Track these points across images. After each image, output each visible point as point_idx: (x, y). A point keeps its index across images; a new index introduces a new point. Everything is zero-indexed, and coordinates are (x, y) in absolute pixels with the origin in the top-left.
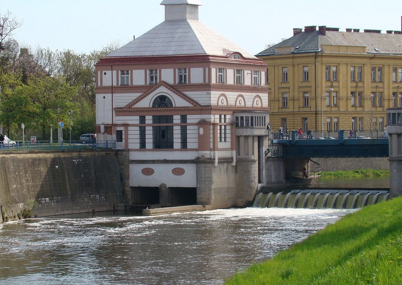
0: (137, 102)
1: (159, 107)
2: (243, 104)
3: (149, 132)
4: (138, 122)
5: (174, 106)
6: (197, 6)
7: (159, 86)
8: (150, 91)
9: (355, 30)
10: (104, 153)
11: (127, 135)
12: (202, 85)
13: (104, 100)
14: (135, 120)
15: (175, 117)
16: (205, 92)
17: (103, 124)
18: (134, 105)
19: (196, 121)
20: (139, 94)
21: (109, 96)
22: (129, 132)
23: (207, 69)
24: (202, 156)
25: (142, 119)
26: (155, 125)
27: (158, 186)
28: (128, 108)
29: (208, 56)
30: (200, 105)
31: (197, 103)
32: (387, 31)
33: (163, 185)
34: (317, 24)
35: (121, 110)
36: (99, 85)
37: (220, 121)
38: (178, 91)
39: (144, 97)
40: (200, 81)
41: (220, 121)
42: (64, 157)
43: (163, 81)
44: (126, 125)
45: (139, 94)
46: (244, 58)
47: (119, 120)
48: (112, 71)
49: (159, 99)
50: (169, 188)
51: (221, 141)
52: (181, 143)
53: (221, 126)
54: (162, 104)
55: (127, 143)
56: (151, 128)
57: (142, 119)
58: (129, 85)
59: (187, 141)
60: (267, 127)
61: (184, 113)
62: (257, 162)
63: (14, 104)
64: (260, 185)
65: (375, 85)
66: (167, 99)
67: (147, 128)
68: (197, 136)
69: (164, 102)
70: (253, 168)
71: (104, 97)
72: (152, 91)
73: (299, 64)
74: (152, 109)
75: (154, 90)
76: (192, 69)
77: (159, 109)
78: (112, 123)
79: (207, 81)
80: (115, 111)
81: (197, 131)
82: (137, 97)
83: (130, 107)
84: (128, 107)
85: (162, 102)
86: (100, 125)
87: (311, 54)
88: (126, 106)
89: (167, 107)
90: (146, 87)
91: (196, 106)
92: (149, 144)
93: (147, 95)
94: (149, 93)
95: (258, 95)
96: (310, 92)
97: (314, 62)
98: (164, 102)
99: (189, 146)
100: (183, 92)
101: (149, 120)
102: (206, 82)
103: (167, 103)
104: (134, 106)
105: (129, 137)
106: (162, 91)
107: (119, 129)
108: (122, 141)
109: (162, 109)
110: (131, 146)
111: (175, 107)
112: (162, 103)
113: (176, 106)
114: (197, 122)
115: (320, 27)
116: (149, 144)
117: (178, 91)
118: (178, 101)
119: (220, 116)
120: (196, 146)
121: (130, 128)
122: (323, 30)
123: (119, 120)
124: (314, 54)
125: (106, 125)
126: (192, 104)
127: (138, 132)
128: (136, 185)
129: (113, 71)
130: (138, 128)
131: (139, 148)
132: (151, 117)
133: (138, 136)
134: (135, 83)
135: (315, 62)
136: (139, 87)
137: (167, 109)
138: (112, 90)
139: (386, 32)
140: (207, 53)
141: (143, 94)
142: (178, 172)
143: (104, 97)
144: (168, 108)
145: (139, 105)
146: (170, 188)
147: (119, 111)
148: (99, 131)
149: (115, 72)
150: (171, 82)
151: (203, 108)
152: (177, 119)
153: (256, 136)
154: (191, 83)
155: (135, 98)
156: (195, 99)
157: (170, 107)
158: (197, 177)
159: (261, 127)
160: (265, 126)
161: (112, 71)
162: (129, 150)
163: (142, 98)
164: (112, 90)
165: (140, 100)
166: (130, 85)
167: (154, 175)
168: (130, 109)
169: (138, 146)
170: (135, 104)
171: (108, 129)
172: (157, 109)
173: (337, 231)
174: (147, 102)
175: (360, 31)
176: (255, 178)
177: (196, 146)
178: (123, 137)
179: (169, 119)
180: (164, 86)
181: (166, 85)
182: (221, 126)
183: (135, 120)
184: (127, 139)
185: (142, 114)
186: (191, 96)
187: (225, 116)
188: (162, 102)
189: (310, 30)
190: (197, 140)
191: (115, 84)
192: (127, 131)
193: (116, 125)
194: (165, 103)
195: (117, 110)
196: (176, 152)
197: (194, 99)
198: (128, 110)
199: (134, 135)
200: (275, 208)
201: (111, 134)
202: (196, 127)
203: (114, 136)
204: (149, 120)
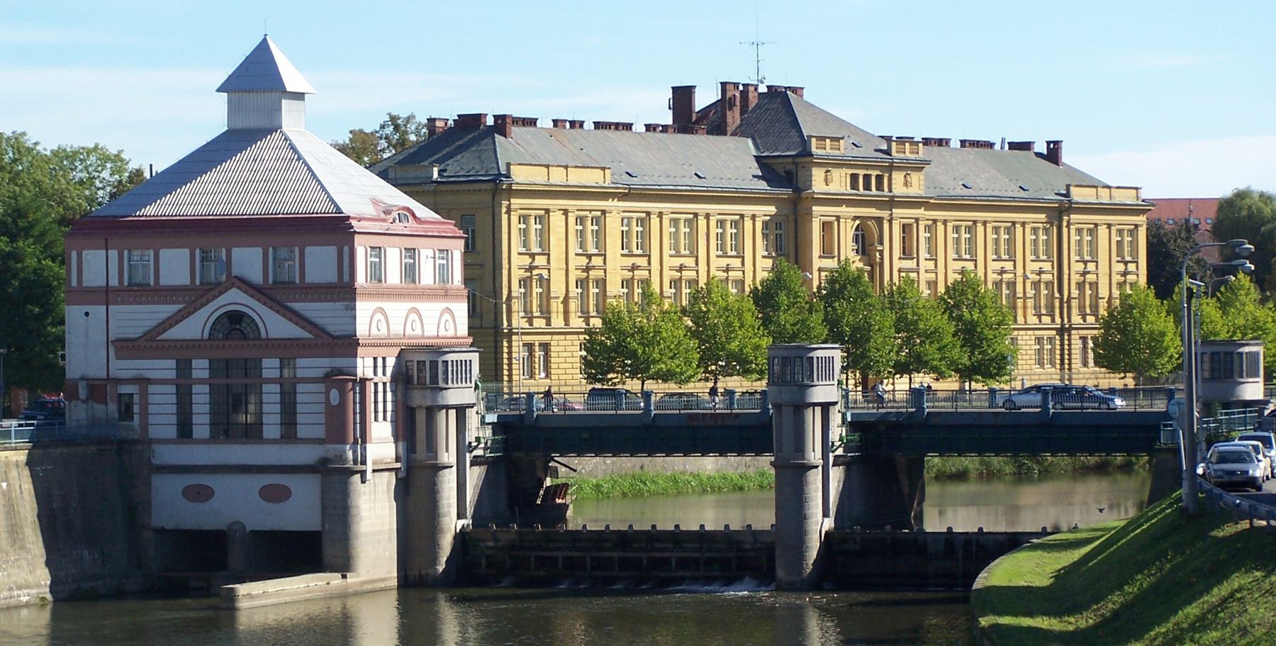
0: (171, 326)
1: (226, 338)
2: (418, 332)
3: (201, 398)
4: (172, 374)
5: (263, 335)
6: (303, 94)
7: (227, 289)
8: (204, 300)
9: (573, 124)
10: (93, 448)
11: (145, 405)
12: (334, 288)
13: (87, 320)
14: (164, 368)
15: (266, 363)
16: (339, 305)
17: (83, 378)
18: (163, 333)
19: (319, 373)
20: (175, 308)
21: (98, 311)
22: (151, 399)
23: (346, 249)
24: (336, 456)
25: (184, 368)
26: (214, 381)
27: (224, 528)
28: (147, 340)
29: (348, 218)
30: (329, 334)
31: (323, 331)
32: (645, 125)
33: (237, 526)
34: (489, 110)
35: (131, 344)
36: (74, 283)
37: (375, 374)
38: (279, 303)
39: (190, 314)
40: (330, 276)
41: (375, 374)
42: (17, 461)
43: (236, 277)
44: (143, 382)
45: (175, 308)
46: (419, 219)
47: (125, 368)
48: (107, 250)
49: (226, 320)
50: (252, 532)
51: (376, 420)
52: (281, 424)
53: (376, 384)
54: (234, 332)
55: (145, 425)
56: (206, 388)
57: (184, 368)
58: (149, 285)
59: (295, 419)
60: (474, 386)
61: (287, 350)
62: (455, 468)
63: (583, 468)
64: (461, 522)
65: (629, 262)
66: (246, 319)
67: (196, 389)
68: (322, 408)
69: (238, 327)
70: (447, 482)
71: (87, 314)
72: (208, 301)
73: (450, 210)
74: (208, 344)
75: (215, 297)
76: (308, 250)
77: (227, 343)
78: (106, 377)
79: (346, 278)
80: (115, 347)
81: (322, 398)
82: (169, 315)
83: (152, 339)
84: (148, 337)
85: (234, 327)
86: (75, 380)
87: (483, 186)
88: (141, 337)
89: (245, 337)
90: (192, 290)
91: (320, 337)
92: (201, 427)
93: (196, 310)
94: (203, 306)
95: (447, 308)
96: (481, 278)
97: (491, 206)
98: (238, 327)
99: (302, 432)
100: (289, 304)
101: (200, 367)
102: (345, 281)
103: (245, 329)
104: (164, 335)
105: (152, 409)
106: (235, 299)
107: (125, 389)
108: (132, 419)
109: (234, 343)
110: (154, 432)
111: (268, 339)
112: (233, 330)
113: (270, 336)
114: (322, 376)
115: (496, 117)
116: (201, 427)
117: (279, 303)
118: (275, 325)
119: (375, 359)
120: (319, 432)
121: (152, 388)
122: (502, 124)
123: (125, 368)
124: (490, 186)
125: (92, 379)
126: (310, 332)
127: (173, 399)
128: (169, 526)
129: (110, 251)
130: (173, 389)
131: (174, 435)
132: (205, 363)
133: (173, 409)
134: (164, 281)
135: (493, 205)
136: (176, 290)
137: (245, 343)
138: (106, 295)
139: (644, 128)
140: (344, 211)
141: (185, 308)
142: (276, 494)
143: (87, 314)
144: (249, 342)
145: (178, 332)
146: (254, 532)
147: (126, 347)
148: (72, 395)
149: (113, 254)
150: (256, 276)
151: (336, 341)
152: (270, 367)
153: (452, 407)
154: (306, 282)
155: (163, 316)
156: (319, 321)
157: (254, 339)
158: (324, 508)
159: (460, 385)
160: (471, 382)
161: (107, 250)
162: (151, 442)
163: (183, 318)
164: (106, 295)
165: (178, 322)
166: (152, 284)
167: (214, 503)
168: (151, 343)
169: (172, 432)
170: (164, 331)
171: (98, 389)
172: (221, 344)
173: (8, 532)
174: (195, 327)
175: (585, 126)
176: (449, 506)
177: (319, 432)
178: (136, 409)
179: (251, 368)
180: (239, 288)
181: (242, 285)
182: (376, 384)
183: (164, 368)
184: (145, 413)
185: (183, 353)
186: (307, 314)
187: (384, 359)
188: (234, 327)
189: (470, 123)
190: (322, 419)
191: (114, 282)
192: (144, 395)
193: (119, 381)
194: (243, 329)
195: (116, 344)
196: (270, 446)
197: (313, 320)
198: (148, 344)
199: (162, 404)
200: (354, 555)
201: (102, 403)
202: (321, 387)
203: (113, 407)
204: (200, 367)
